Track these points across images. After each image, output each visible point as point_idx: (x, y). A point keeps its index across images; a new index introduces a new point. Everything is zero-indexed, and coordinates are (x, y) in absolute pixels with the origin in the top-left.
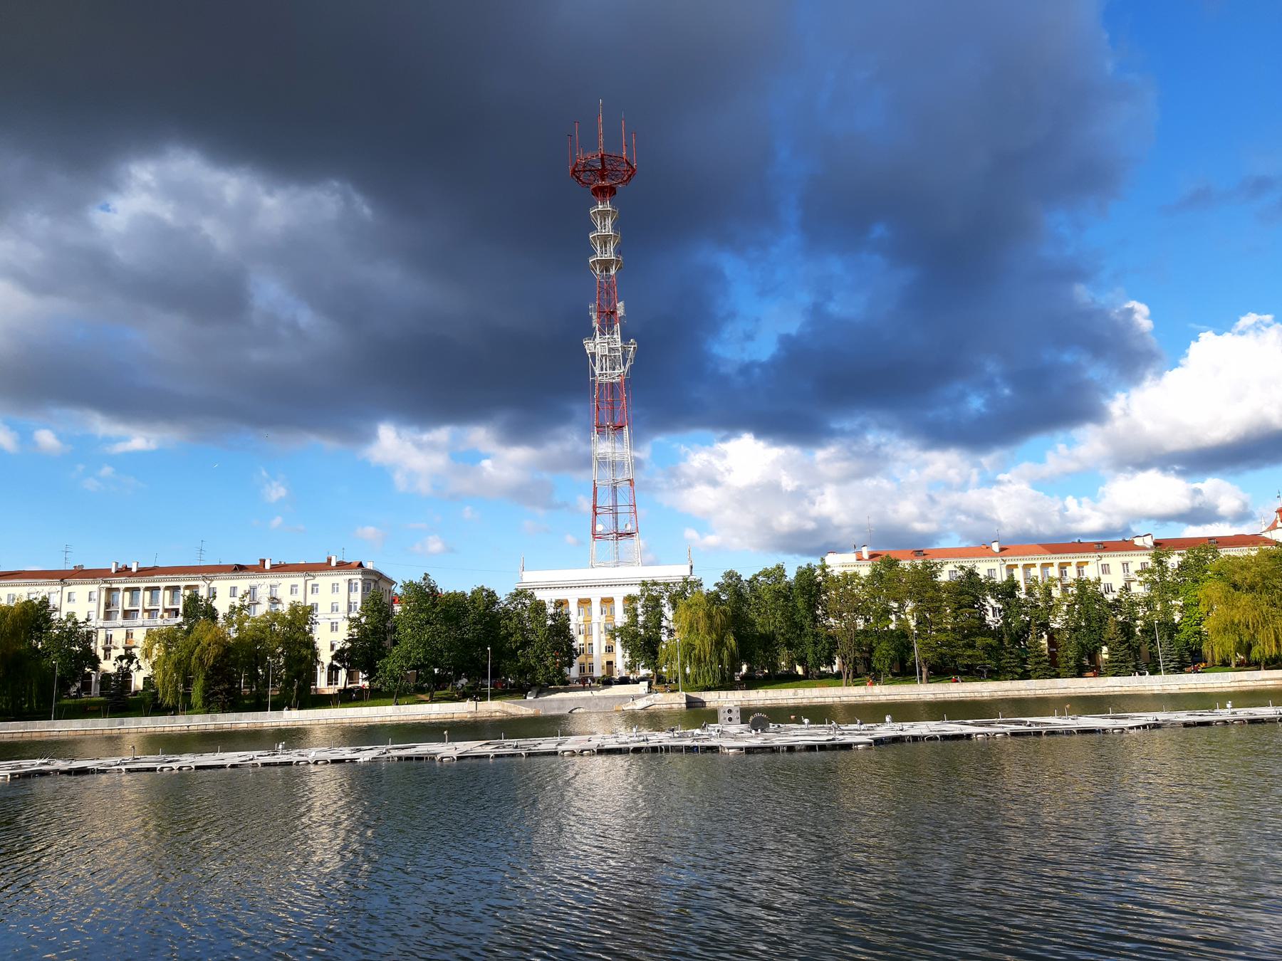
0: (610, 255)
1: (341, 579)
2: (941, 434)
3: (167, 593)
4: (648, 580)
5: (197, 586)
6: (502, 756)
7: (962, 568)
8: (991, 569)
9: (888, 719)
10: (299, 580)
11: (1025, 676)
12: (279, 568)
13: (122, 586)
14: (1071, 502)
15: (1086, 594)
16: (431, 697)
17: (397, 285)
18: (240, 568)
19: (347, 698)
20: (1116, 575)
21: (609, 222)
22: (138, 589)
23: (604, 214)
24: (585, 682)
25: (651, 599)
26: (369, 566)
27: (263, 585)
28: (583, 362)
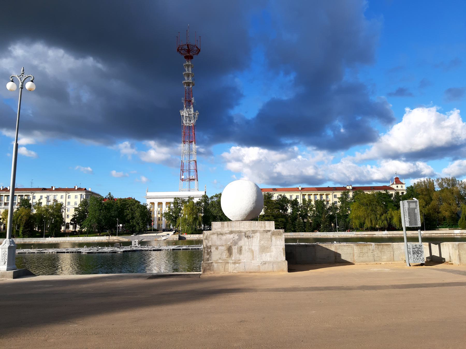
1: (78, 194)
2: (320, 146)
6: (92, 253)
7: (281, 195)
10: (64, 194)
11: (295, 231)
12: (58, 190)
13: (4, 194)
14: (369, 167)
15: (320, 204)
18: (44, 189)
20: (333, 199)
23: (188, 66)
24: (156, 231)
26: (90, 190)
27: (52, 195)
28: (180, 118)
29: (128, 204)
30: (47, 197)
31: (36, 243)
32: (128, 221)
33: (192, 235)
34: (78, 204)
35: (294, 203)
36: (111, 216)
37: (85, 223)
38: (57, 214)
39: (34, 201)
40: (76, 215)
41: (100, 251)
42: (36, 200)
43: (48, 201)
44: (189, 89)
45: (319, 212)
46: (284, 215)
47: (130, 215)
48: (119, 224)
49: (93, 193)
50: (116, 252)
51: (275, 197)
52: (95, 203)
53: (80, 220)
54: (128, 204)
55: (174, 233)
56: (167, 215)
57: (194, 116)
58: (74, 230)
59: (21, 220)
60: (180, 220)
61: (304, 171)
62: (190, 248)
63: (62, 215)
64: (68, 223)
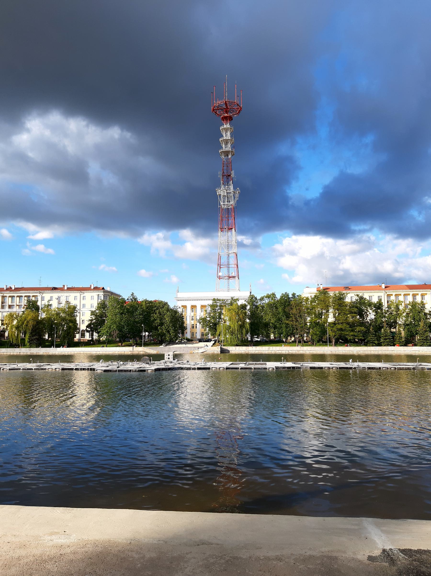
0: (229, 148)
1: (95, 294)
2: (403, 232)
3: (18, 298)
4: (216, 298)
5: (37, 296)
7: (358, 295)
8: (374, 297)
9: (350, 361)
10: (77, 294)
11: (379, 345)
16: (122, 344)
17: (148, 165)
18: (55, 289)
19: (90, 343)
21: (229, 133)
22: (14, 296)
23: (226, 130)
24: (189, 341)
25: (217, 306)
26: (108, 289)
28: (216, 198)
29: (155, 307)
30: (58, 298)
31: (45, 354)
32: (156, 328)
33: (238, 347)
34: (94, 307)
35: (378, 306)
36: (135, 322)
37: (104, 329)
38: (69, 318)
39: (43, 302)
40: (92, 320)
41: (121, 368)
42: (45, 302)
43: (59, 303)
44: (227, 159)
45: (414, 319)
46: (363, 323)
47: (158, 321)
48: (145, 331)
49: (112, 293)
50: (144, 371)
51: (350, 297)
52: (116, 305)
53: (97, 326)
54: (155, 307)
55: (214, 344)
56: (203, 321)
57: (234, 195)
58: (90, 339)
59: (27, 325)
60: (221, 328)
61: (379, 267)
62: (252, 367)
63: (75, 320)
64: (83, 331)
